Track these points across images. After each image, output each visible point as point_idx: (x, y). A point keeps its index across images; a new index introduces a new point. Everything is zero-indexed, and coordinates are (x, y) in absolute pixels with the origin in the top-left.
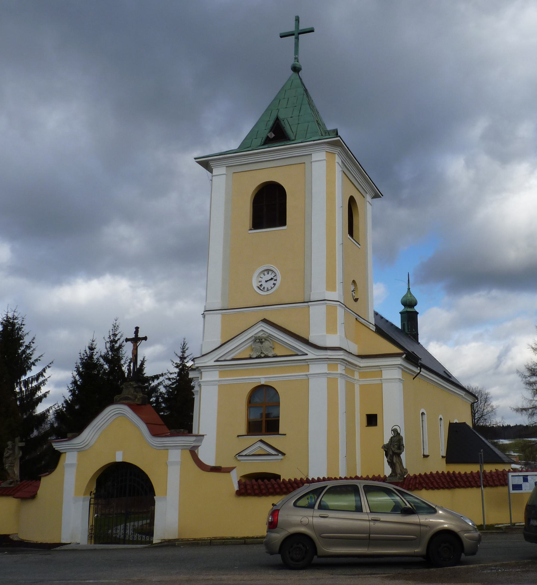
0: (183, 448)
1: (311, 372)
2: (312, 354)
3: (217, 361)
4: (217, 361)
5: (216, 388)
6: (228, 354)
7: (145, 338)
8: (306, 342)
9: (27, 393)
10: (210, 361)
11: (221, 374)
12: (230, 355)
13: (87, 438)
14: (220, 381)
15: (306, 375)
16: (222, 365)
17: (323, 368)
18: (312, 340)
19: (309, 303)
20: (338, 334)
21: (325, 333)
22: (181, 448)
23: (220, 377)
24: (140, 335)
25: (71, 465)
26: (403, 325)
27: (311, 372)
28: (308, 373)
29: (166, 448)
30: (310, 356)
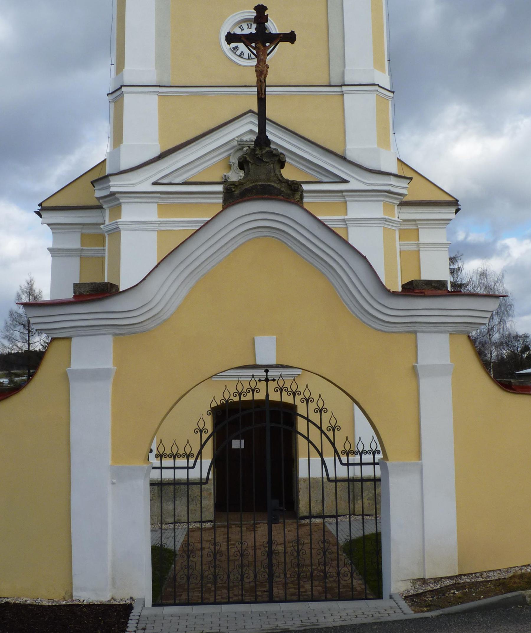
0: (456, 330)
1: (351, 215)
2: (357, 182)
3: (155, 183)
4: (155, 183)
5: (154, 236)
6: (175, 175)
7: (290, 37)
8: (343, 158)
9: (267, 44)
10: (142, 182)
11: (162, 209)
12: (180, 175)
13: (175, 286)
14: (162, 223)
15: (344, 220)
16: (163, 196)
17: (375, 210)
18: (351, 155)
19: (344, 88)
20: (392, 150)
21: (376, 146)
22: (451, 329)
23: (160, 216)
24: (273, 27)
25: (96, 375)
26: (301, 186)
27: (351, 215)
28: (346, 217)
29: (412, 329)
30: (354, 185)
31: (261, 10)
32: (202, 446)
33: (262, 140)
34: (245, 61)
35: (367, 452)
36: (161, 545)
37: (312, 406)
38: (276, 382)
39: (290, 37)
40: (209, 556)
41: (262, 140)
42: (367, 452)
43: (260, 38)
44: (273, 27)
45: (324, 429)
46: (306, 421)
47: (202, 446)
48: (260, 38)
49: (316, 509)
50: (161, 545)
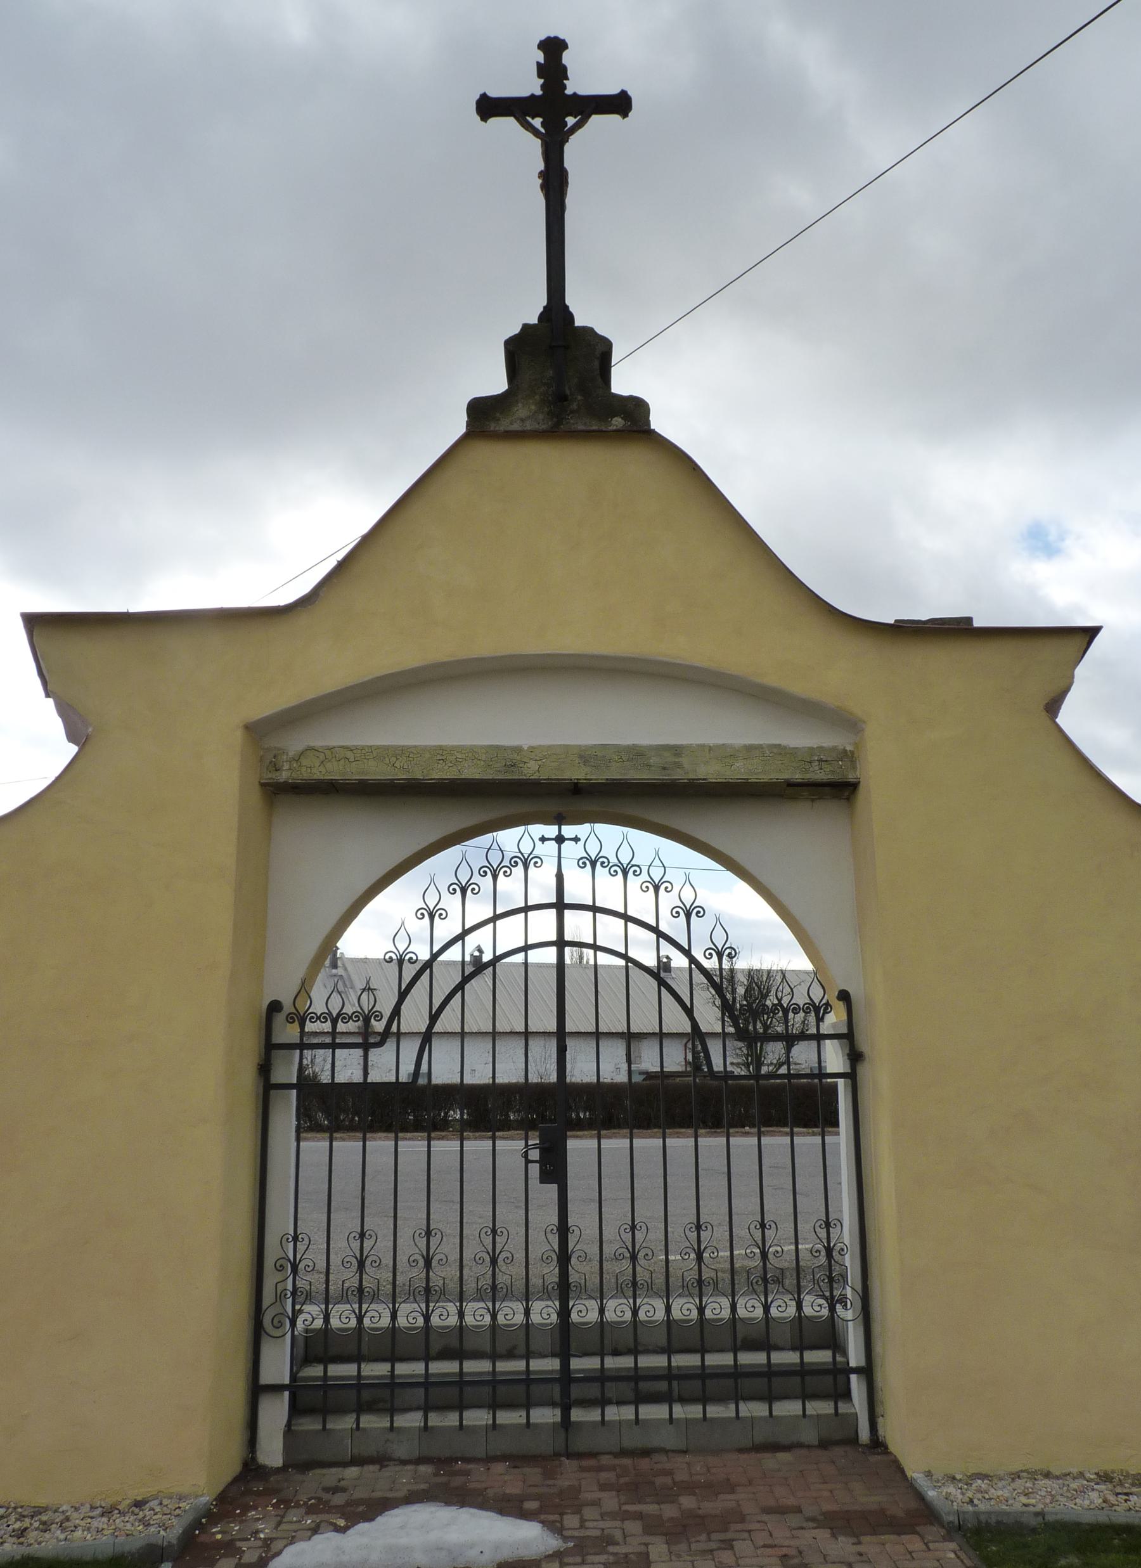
31: (553, 47)
32: (403, 995)
33: (556, 309)
34: (518, 146)
35: (318, 1018)
36: (429, 1140)
37: (668, 901)
38: (581, 843)
39: (620, 104)
40: (412, 1263)
41: (556, 309)
42: (318, 1018)
43: (554, 108)
44: (582, 81)
45: (698, 954)
46: (654, 936)
47: (403, 995)
48: (554, 108)
49: (612, 1021)
50: (429, 1140)
